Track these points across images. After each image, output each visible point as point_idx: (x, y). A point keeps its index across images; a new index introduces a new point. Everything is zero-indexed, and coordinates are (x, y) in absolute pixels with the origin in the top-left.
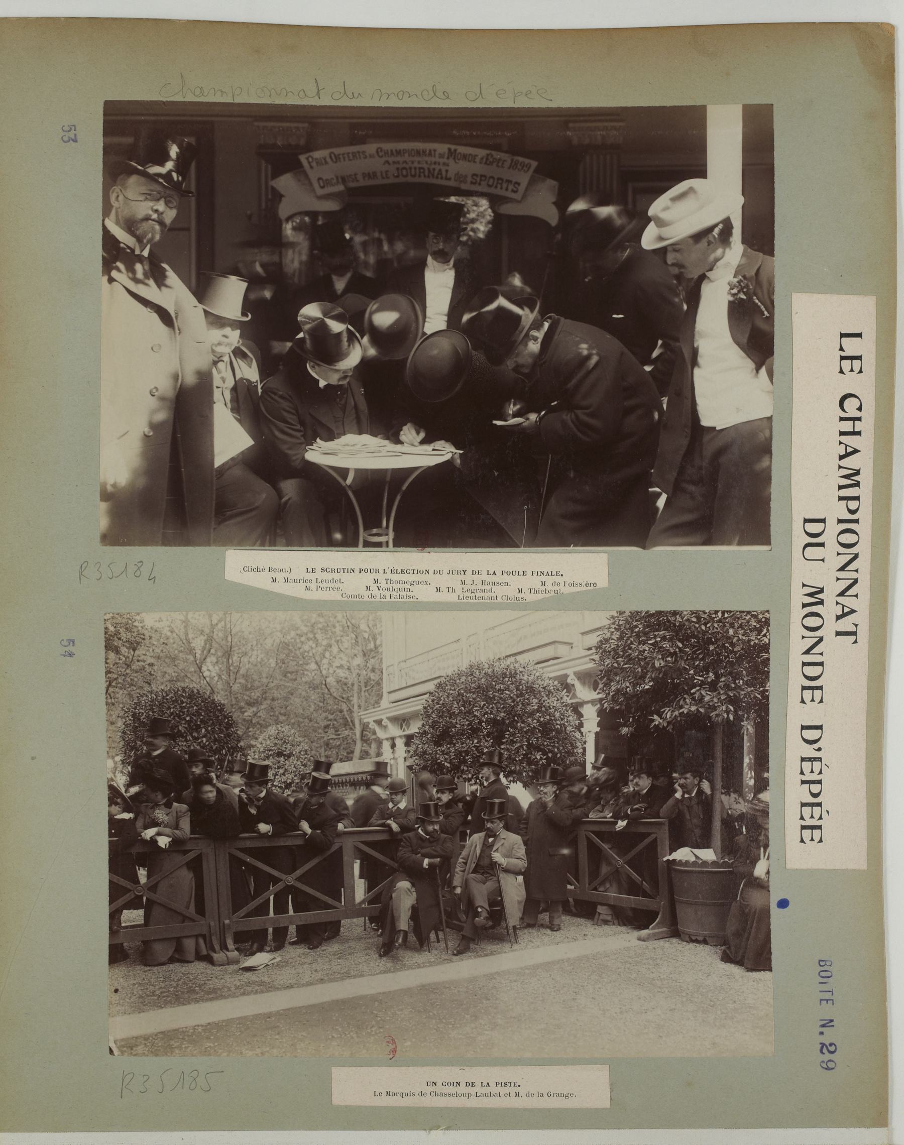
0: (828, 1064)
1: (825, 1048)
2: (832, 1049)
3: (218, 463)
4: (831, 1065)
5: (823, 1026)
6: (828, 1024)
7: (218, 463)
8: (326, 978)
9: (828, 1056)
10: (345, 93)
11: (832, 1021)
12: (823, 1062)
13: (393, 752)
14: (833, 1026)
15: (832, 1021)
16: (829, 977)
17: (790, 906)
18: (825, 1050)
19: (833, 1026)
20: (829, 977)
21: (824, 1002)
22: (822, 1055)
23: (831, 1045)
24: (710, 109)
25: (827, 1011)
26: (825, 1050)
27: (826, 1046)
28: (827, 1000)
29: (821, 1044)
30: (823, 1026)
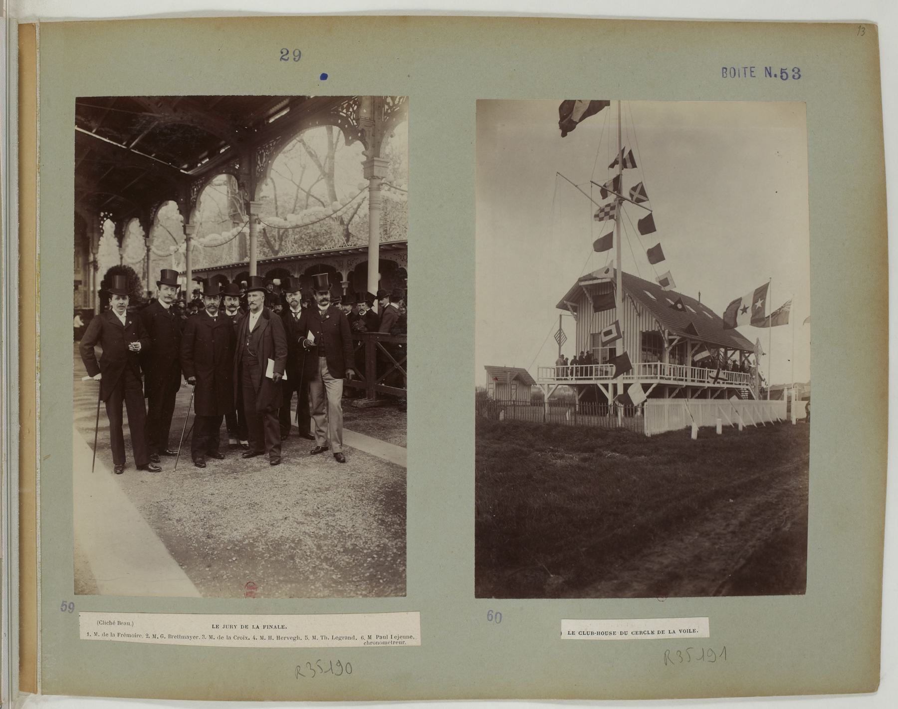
0: (296, 55)
1: (283, 57)
2: (285, 52)
3: (377, 313)
4: (297, 53)
5: (770, 74)
6: (768, 72)
7: (377, 313)
8: (200, 475)
9: (291, 55)
10: (292, 180)
11: (766, 68)
12: (294, 59)
13: (120, 246)
14: (770, 68)
15: (766, 68)
16: (735, 70)
17: (328, 78)
18: (285, 57)
19: (770, 68)
20: (735, 70)
21: (753, 74)
22: (289, 60)
23: (282, 53)
24: (611, 101)
25: (760, 72)
26: (285, 57)
27: (283, 56)
28: (752, 72)
29: (281, 60)
30: (770, 74)
